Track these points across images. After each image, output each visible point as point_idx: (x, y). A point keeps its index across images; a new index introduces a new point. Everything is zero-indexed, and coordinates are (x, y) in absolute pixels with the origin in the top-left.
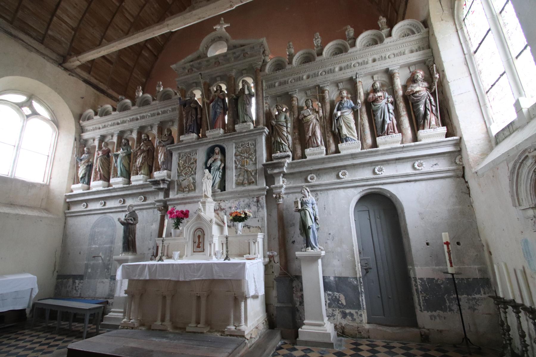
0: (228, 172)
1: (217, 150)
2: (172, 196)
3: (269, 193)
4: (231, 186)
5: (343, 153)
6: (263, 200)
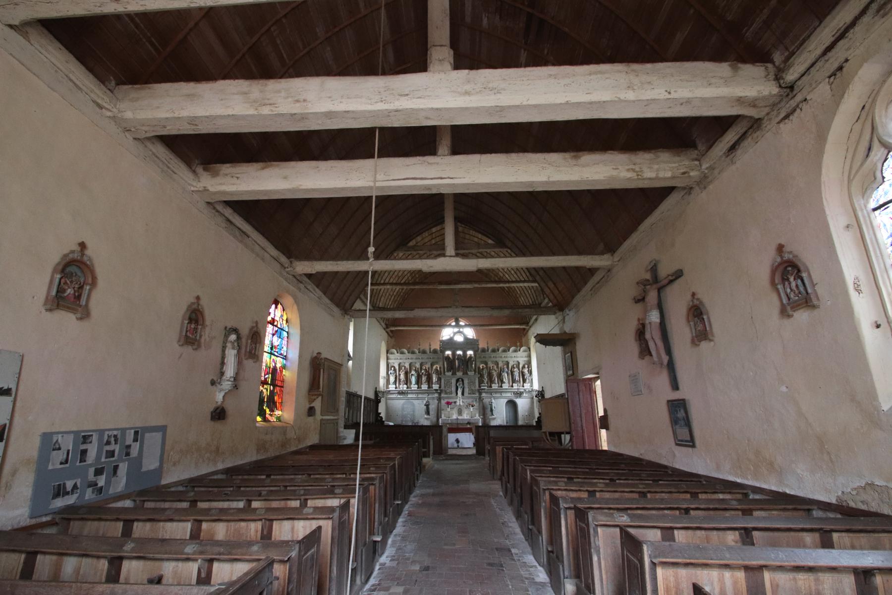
0: (465, 390)
2: (442, 395)
3: (480, 398)
4: (466, 394)
5: (504, 387)
6: (478, 400)
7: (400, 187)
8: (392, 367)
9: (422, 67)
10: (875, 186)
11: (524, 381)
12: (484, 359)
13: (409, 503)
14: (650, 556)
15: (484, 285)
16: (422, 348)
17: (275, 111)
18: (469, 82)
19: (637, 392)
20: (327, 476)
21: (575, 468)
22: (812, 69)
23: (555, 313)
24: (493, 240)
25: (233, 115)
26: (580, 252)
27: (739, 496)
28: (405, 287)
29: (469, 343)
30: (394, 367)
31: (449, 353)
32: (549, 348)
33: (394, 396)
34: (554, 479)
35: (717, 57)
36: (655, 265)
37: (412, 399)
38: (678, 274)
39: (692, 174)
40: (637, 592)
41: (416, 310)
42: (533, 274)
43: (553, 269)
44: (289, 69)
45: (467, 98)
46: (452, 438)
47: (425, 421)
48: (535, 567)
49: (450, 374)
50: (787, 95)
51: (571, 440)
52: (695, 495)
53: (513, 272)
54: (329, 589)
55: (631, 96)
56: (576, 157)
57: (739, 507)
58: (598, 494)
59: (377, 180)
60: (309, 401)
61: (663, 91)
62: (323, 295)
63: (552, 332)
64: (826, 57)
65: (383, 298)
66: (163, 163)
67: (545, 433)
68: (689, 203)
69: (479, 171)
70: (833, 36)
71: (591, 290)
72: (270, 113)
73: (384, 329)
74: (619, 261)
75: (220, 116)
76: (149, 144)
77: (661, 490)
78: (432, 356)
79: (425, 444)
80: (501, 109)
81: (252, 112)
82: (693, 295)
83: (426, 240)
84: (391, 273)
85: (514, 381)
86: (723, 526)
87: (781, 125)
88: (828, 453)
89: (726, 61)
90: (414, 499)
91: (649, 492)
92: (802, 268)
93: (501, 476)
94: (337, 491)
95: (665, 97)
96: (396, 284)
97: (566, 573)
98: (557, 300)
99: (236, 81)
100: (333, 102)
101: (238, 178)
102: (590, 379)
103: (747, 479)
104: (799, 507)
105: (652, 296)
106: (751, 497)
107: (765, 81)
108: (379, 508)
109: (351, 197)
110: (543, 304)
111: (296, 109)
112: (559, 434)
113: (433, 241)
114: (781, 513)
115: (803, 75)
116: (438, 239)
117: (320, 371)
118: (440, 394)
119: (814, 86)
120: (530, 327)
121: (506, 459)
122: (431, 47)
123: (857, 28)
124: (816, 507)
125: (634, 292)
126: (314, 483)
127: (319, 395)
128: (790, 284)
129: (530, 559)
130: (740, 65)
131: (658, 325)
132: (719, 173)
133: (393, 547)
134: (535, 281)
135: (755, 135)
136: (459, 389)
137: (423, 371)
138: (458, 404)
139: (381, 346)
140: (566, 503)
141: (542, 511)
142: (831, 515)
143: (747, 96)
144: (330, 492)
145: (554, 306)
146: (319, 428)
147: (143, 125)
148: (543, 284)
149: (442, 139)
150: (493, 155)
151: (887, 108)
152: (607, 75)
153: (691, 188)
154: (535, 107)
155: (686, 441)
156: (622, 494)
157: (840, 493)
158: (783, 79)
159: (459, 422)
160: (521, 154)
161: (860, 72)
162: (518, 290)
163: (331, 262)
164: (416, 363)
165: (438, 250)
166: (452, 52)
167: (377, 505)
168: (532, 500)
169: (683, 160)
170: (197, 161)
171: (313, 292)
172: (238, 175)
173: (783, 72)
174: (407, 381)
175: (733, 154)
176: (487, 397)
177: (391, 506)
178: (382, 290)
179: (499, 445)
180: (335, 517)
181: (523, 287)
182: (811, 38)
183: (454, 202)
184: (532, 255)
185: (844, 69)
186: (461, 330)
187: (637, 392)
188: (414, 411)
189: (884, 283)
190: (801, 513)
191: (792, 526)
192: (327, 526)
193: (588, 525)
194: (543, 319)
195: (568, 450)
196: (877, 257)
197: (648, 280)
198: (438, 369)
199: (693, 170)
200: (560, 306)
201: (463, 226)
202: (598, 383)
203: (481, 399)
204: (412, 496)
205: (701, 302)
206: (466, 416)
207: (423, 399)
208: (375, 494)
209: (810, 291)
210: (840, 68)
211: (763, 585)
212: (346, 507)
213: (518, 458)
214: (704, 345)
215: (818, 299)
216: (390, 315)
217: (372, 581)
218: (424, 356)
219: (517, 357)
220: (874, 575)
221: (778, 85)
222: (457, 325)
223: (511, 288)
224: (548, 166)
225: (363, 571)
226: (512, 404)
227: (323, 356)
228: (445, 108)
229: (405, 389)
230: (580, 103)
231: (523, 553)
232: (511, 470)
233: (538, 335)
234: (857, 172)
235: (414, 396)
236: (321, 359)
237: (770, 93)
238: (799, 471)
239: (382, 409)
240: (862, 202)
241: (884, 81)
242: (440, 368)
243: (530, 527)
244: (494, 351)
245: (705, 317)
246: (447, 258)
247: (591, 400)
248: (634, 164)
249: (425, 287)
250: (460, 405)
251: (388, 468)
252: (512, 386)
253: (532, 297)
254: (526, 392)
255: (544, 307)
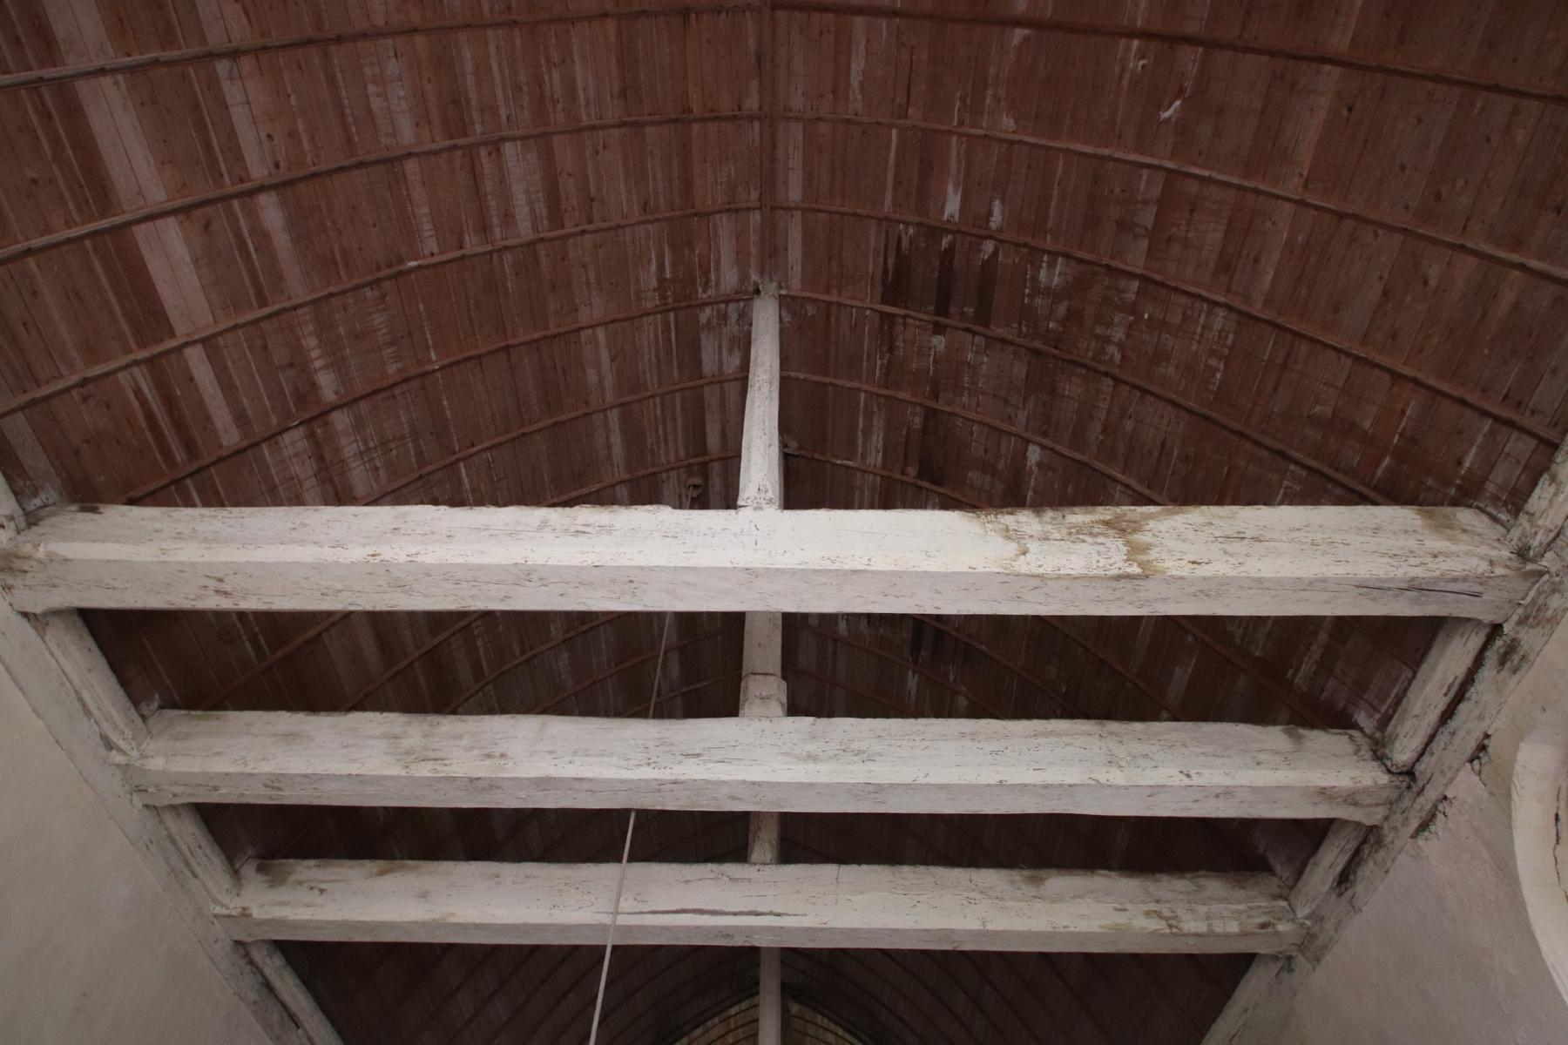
7: (665, 929)
9: (728, 706)
17: (441, 772)
18: (814, 738)
25: (357, 775)
35: (1257, 714)
44: (487, 684)
45: (811, 767)
50: (1409, 787)
55: (1117, 777)
59: (619, 911)
61: (1175, 772)
66: (182, 854)
68: (1295, 994)
70: (1446, 695)
72: (429, 775)
75: (334, 775)
76: (170, 819)
81: (396, 771)
83: (714, 1034)
87: (1421, 842)
89: (1275, 723)
95: (1183, 783)
99: (385, 714)
100: (555, 761)
101: (322, 891)
107: (1358, 761)
111: (484, 770)
115: (1421, 754)
119: (1449, 774)
122: (747, 675)
130: (1301, 731)
132: (1336, 930)
143: (1334, 787)
147: (176, 783)
149: (760, 829)
154: (942, 788)
158: (1390, 759)
166: (784, 685)
169: (1255, 898)
170: (250, 852)
172: (324, 886)
182: (1408, 694)
199: (1280, 919)
221: (1384, 769)
224: (979, 896)
230: (1026, 785)
248: (1157, 902)
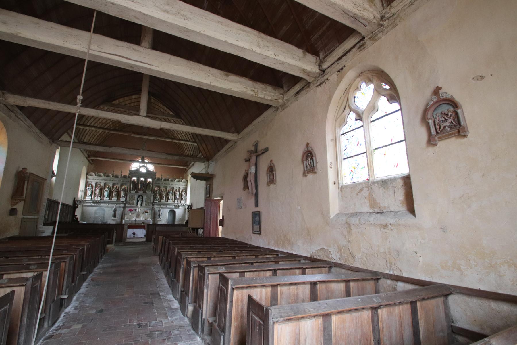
0: (143, 202)
1: (141, 196)
2: (127, 205)
4: (144, 205)
5: (169, 202)
6: (151, 209)
7: (110, 59)
8: (90, 184)
10: (344, 124)
11: (182, 199)
12: (158, 185)
13: (93, 273)
14: (231, 285)
15: (163, 139)
16: (115, 173)
18: (168, 4)
19: (239, 207)
20: (24, 258)
21: (203, 246)
22: (332, 65)
23: (204, 162)
24: (173, 113)
26: (222, 130)
27: (275, 256)
28: (107, 131)
29: (149, 174)
30: (92, 185)
31: (135, 178)
32: (198, 181)
33: (90, 204)
34: (191, 252)
36: (257, 143)
37: (103, 206)
38: (266, 150)
39: (279, 101)
40: (223, 304)
41: (114, 148)
42: (195, 137)
43: (206, 136)
45: (166, 15)
46: (130, 232)
47: (111, 221)
48: (173, 300)
49: (134, 192)
50: (322, 75)
51: (203, 232)
52: (257, 256)
53: (183, 135)
54: (19, 333)
55: (258, 50)
56: (226, 75)
57: (274, 260)
58: (212, 259)
60: (12, 204)
61: (273, 53)
62: (33, 125)
63: (201, 172)
64: (338, 62)
65: (87, 136)
67: (189, 228)
68: (276, 116)
69: (169, 66)
70: (342, 53)
71: (225, 152)
73: (86, 158)
74: (241, 138)
77: (242, 255)
78: (122, 179)
79: (110, 236)
80: (188, 31)
82: (271, 161)
83: (127, 102)
84: (97, 120)
85: (175, 199)
86: (266, 269)
87: (317, 88)
88: (310, 236)
89: (302, 49)
90: (96, 271)
91: (237, 256)
92: (314, 155)
93: (160, 254)
94: (32, 267)
95: (273, 57)
96: (100, 128)
97: (190, 301)
98: (206, 155)
102: (218, 200)
103: (279, 248)
104: (297, 259)
105: (253, 159)
106: (280, 256)
108: (67, 278)
109: (68, 56)
110: (198, 156)
112: (197, 229)
113: (132, 105)
114: (290, 262)
115: (329, 67)
116: (135, 104)
117: (24, 183)
118: (125, 204)
119: (332, 74)
120: (189, 168)
121: (164, 243)
123: (351, 53)
124: (302, 259)
125: (245, 155)
126: (11, 263)
127: (23, 200)
128: (308, 161)
129: (171, 297)
130: (307, 53)
131: (254, 173)
133: (77, 301)
134: (195, 142)
135: (307, 90)
136: (139, 202)
137: (114, 189)
138: (137, 211)
139: (82, 169)
140: (195, 264)
141: (181, 270)
142: (307, 262)
144: (27, 268)
145: (204, 158)
146: (20, 225)
148: (199, 144)
150: (179, 58)
151: (353, 92)
152: (248, 34)
153: (278, 108)
155: (257, 232)
156: (224, 258)
157: (312, 252)
158: (322, 66)
159: (136, 222)
160: (196, 63)
161: (348, 73)
162: (185, 146)
163: (43, 101)
164: (109, 183)
165: (135, 110)
167: (66, 276)
168: (176, 264)
171: (24, 121)
173: (322, 63)
174: (101, 195)
175: (297, 96)
176: (158, 208)
177: (78, 276)
178: (88, 130)
179: (160, 235)
180: (28, 284)
181: (188, 145)
183: (150, 81)
184: (195, 126)
185: (343, 70)
186: (145, 165)
187: (239, 207)
188: (104, 215)
189: (340, 167)
190: (297, 262)
191: (292, 267)
192: (20, 292)
193: (204, 274)
194: (197, 164)
195: (201, 237)
196: (339, 154)
197: (253, 151)
198: (126, 188)
200: (207, 158)
201: (155, 99)
202: (222, 202)
203: (153, 208)
204: (95, 269)
205: (274, 165)
206: (142, 218)
207: (113, 207)
208: (65, 268)
209: (315, 166)
210: (342, 69)
211: (277, 293)
212: (39, 277)
213: (171, 242)
214: (272, 186)
215: (317, 170)
216: (92, 148)
217: (57, 324)
218: (116, 179)
219: (179, 185)
220: (317, 284)
222: (143, 162)
223: (181, 144)
225: (50, 319)
226: (173, 212)
227: (28, 171)
228: (150, 16)
229: (99, 200)
230: (233, 44)
231: (167, 294)
232: (166, 249)
233: (193, 173)
234: (339, 117)
235: (106, 205)
236: (27, 173)
237: (316, 71)
238: (299, 244)
239: (78, 213)
240: (339, 130)
241: (355, 80)
242: (127, 188)
243: (173, 280)
244: (165, 180)
245: (274, 172)
246: (141, 117)
247: (217, 211)
248: (255, 88)
249: (122, 133)
250: (139, 212)
251: (78, 251)
252: (174, 202)
253: (192, 151)
254: (182, 206)
255: (199, 158)
